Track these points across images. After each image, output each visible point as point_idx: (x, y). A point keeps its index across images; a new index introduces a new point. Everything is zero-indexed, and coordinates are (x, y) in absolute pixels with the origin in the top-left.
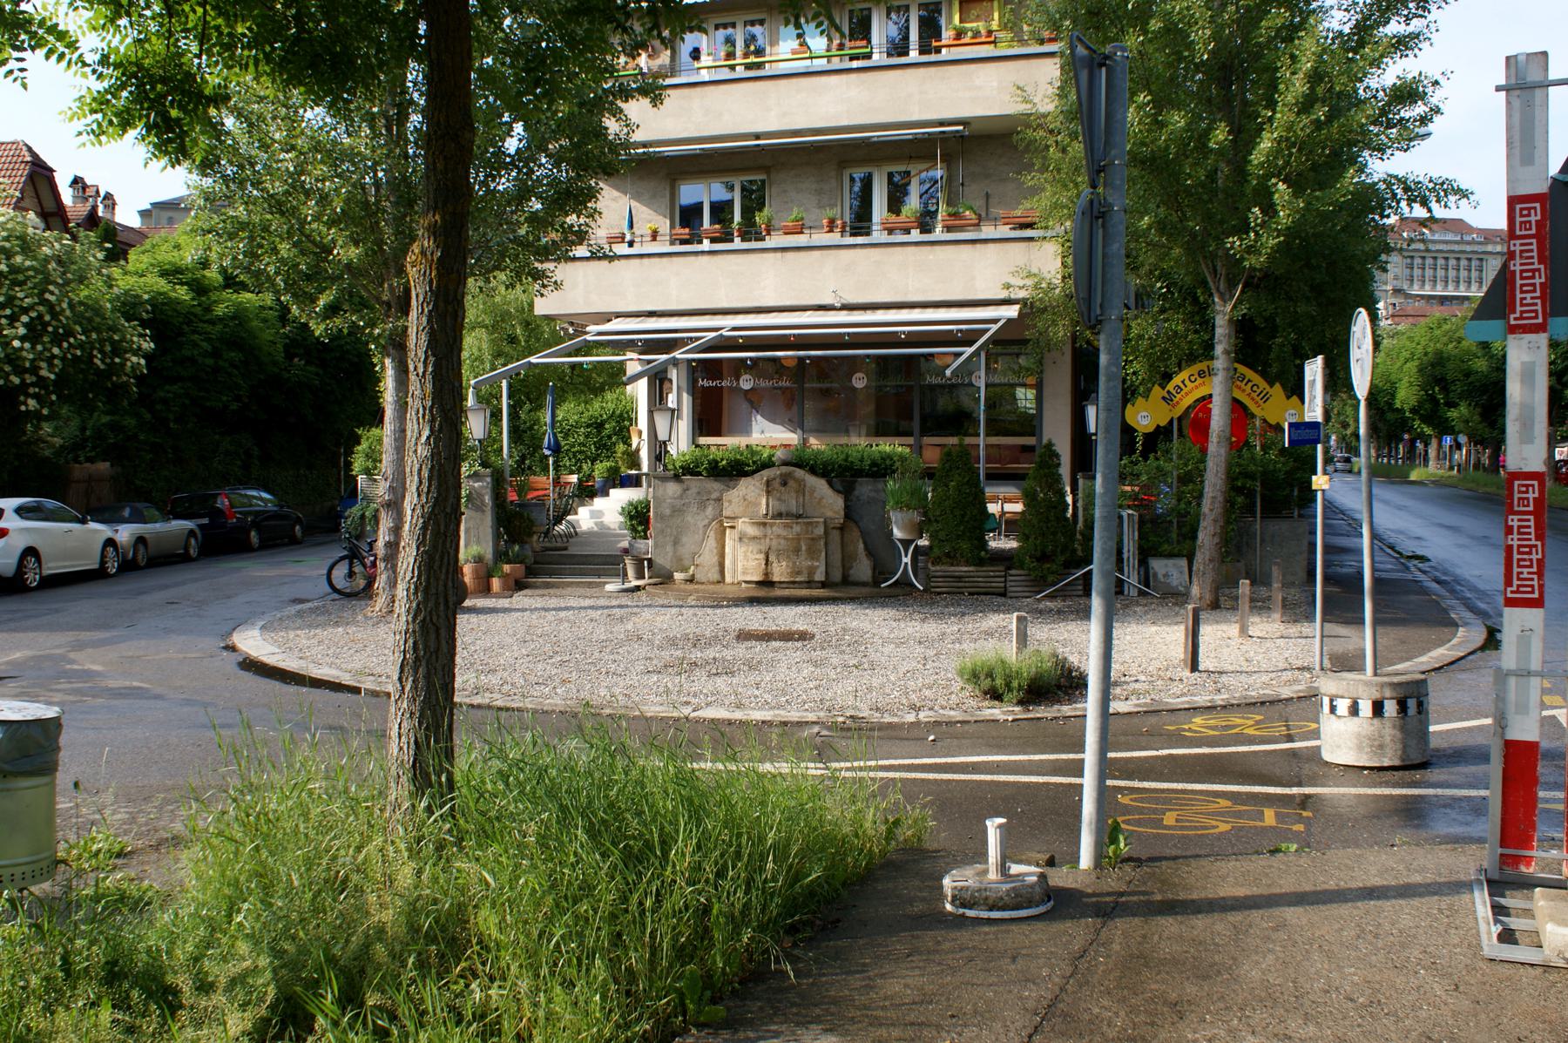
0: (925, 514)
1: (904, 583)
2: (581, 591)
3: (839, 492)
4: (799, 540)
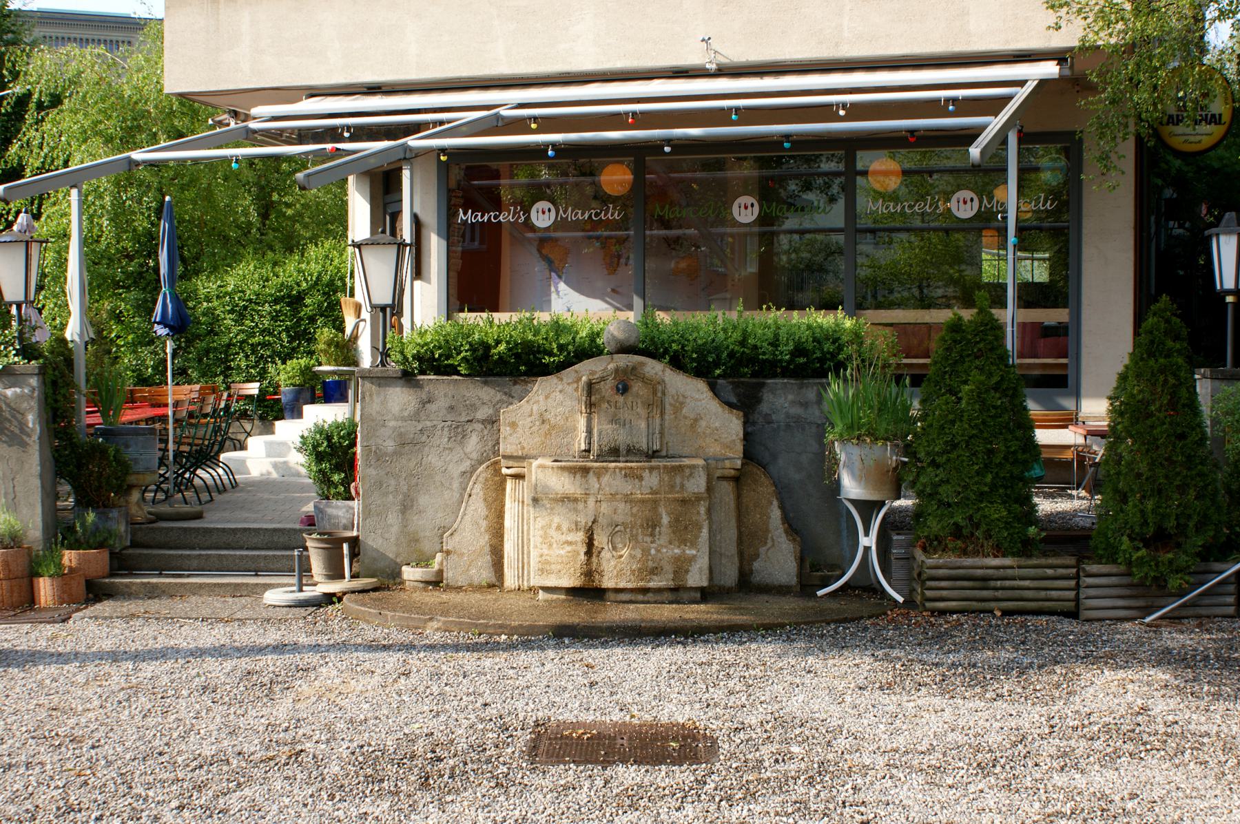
0: (908, 450)
1: (864, 587)
2: (215, 604)
3: (731, 405)
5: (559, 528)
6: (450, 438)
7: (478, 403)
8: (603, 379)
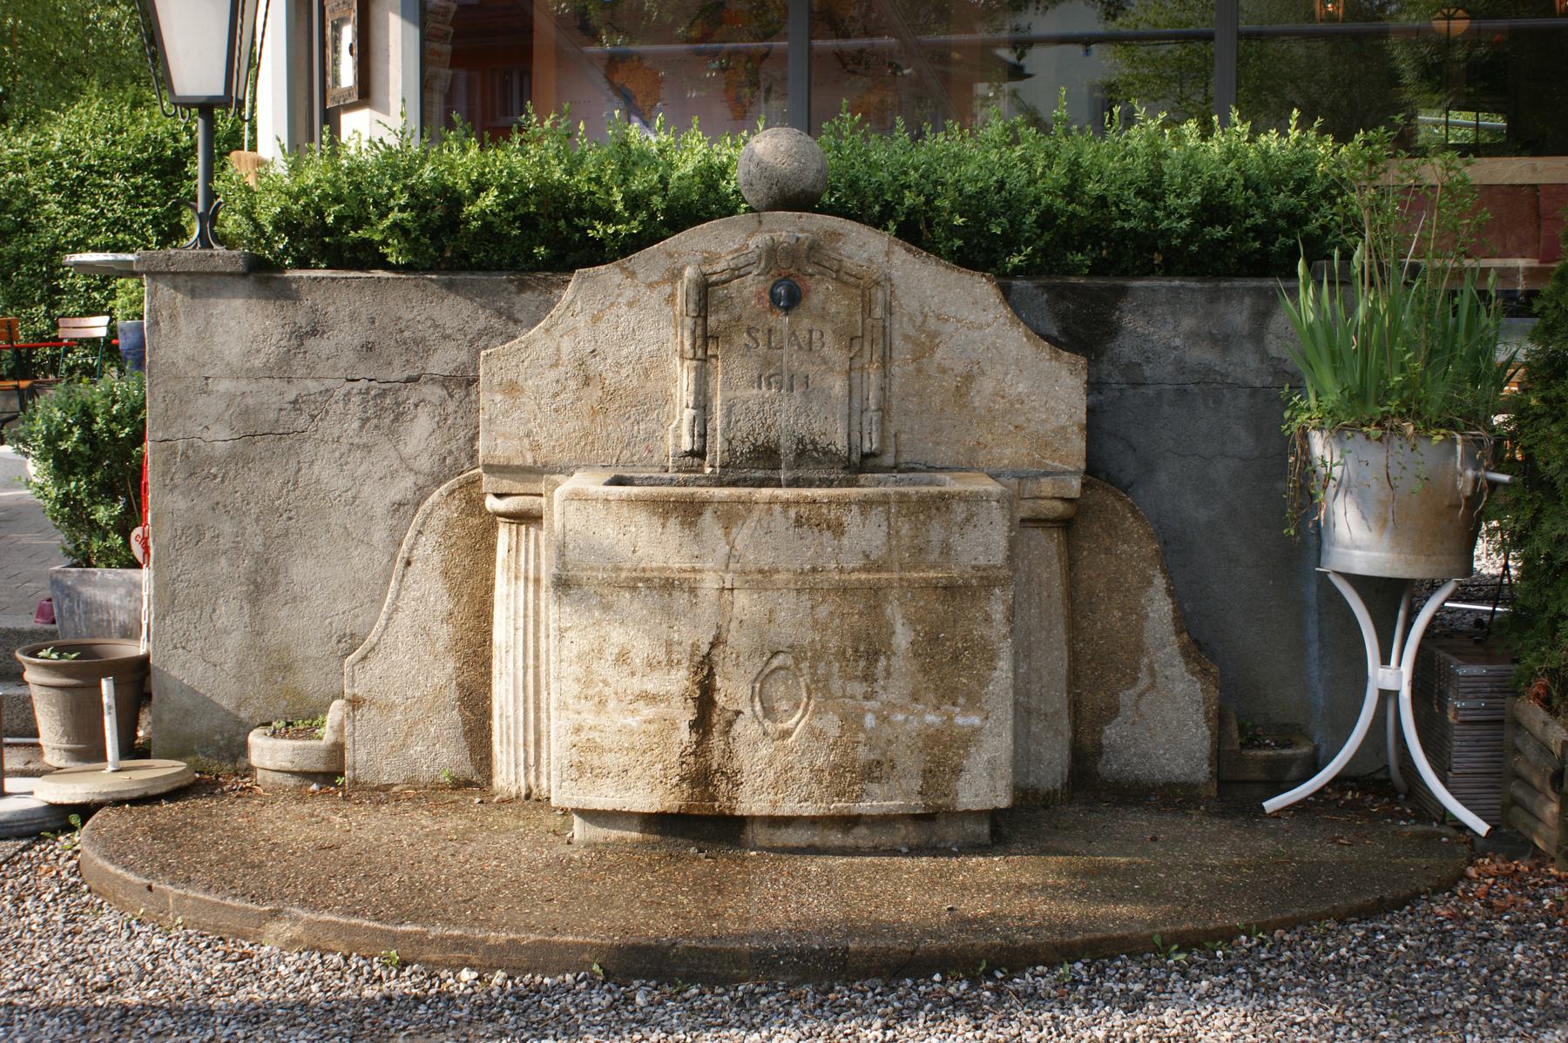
1: (1380, 787)
4: (876, 593)
5: (622, 658)
6: (365, 421)
7: (432, 336)
8: (737, 273)
